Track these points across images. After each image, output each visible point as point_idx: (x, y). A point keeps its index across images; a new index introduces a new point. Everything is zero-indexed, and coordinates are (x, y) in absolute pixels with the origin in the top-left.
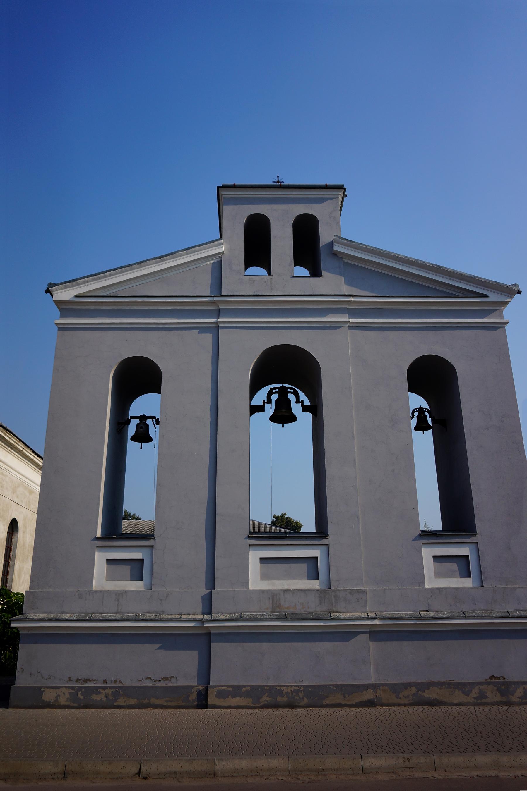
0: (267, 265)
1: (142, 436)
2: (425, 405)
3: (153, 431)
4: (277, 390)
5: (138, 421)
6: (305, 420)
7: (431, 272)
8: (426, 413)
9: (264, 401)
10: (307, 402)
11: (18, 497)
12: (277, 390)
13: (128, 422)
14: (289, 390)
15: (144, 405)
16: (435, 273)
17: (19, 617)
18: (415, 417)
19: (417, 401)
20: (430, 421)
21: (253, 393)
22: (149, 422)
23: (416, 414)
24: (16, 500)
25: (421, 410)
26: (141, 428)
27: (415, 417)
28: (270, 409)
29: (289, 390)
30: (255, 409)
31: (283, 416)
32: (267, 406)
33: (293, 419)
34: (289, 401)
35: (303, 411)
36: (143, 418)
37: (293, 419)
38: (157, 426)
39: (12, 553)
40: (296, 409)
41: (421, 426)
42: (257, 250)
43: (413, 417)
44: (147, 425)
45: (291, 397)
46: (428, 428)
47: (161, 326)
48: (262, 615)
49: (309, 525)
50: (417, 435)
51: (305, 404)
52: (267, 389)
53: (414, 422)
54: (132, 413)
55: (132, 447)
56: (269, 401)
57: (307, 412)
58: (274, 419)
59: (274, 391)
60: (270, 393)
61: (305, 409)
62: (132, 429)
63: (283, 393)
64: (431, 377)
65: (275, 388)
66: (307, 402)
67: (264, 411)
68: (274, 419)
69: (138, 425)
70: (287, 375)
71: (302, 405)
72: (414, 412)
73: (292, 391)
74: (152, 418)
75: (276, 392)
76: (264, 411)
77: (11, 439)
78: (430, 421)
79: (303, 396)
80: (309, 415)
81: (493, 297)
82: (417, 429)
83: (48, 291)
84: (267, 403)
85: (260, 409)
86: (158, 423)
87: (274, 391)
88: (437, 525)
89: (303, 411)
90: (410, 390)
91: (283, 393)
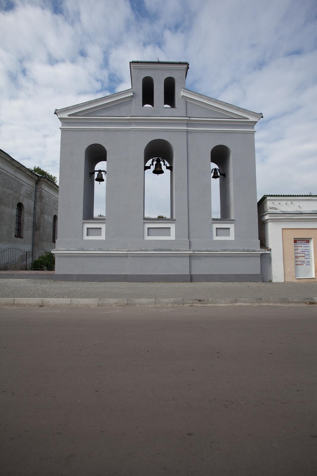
0: (152, 104)
1: (100, 179)
2: (217, 167)
3: (104, 177)
4: (156, 160)
5: (98, 172)
6: (167, 172)
7: (245, 114)
8: (217, 171)
9: (150, 164)
10: (168, 165)
11: (56, 207)
12: (156, 160)
13: (94, 173)
14: (161, 160)
15: (101, 166)
16: (233, 109)
17: (54, 250)
18: (213, 172)
19: (214, 166)
20: (219, 174)
21: (146, 161)
22: (103, 173)
23: (213, 171)
24: (55, 208)
25: (215, 169)
26: (99, 175)
27: (213, 172)
28: (153, 168)
29: (161, 160)
30: (146, 168)
31: (158, 171)
32: (152, 167)
33: (162, 172)
34: (161, 164)
35: (167, 169)
36: (100, 171)
37: (162, 172)
38: (106, 175)
39: (56, 228)
40: (164, 168)
41: (215, 177)
42: (148, 97)
43: (212, 172)
44: (102, 174)
45: (162, 163)
46: (218, 177)
47: (106, 130)
48: (148, 249)
49: (168, 216)
50: (213, 180)
51: (167, 166)
52: (151, 160)
53: (212, 174)
54: (96, 169)
55: (96, 183)
56: (153, 164)
57: (168, 169)
58: (155, 172)
59: (154, 160)
60: (153, 161)
61: (167, 168)
62: (96, 176)
63: (158, 161)
64: (220, 155)
65: (155, 159)
66: (168, 165)
67: (150, 169)
68: (155, 172)
69: (98, 174)
70: (159, 153)
71: (166, 166)
72: (212, 170)
73: (162, 160)
74: (104, 171)
75: (155, 161)
76: (150, 169)
77: (34, 176)
78: (219, 174)
79: (166, 163)
80: (169, 171)
81: (252, 119)
82: (213, 177)
83: (55, 113)
84: (152, 165)
85: (149, 168)
86: (106, 172)
87: (154, 160)
88: (219, 216)
89: (167, 169)
90: (211, 162)
91: (158, 161)
